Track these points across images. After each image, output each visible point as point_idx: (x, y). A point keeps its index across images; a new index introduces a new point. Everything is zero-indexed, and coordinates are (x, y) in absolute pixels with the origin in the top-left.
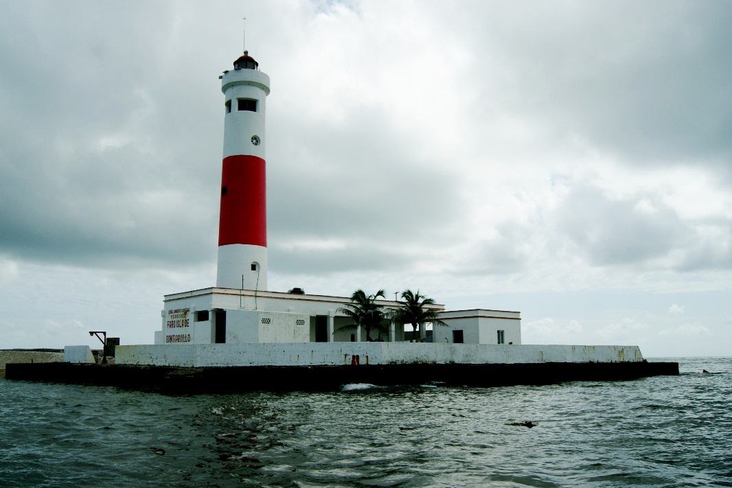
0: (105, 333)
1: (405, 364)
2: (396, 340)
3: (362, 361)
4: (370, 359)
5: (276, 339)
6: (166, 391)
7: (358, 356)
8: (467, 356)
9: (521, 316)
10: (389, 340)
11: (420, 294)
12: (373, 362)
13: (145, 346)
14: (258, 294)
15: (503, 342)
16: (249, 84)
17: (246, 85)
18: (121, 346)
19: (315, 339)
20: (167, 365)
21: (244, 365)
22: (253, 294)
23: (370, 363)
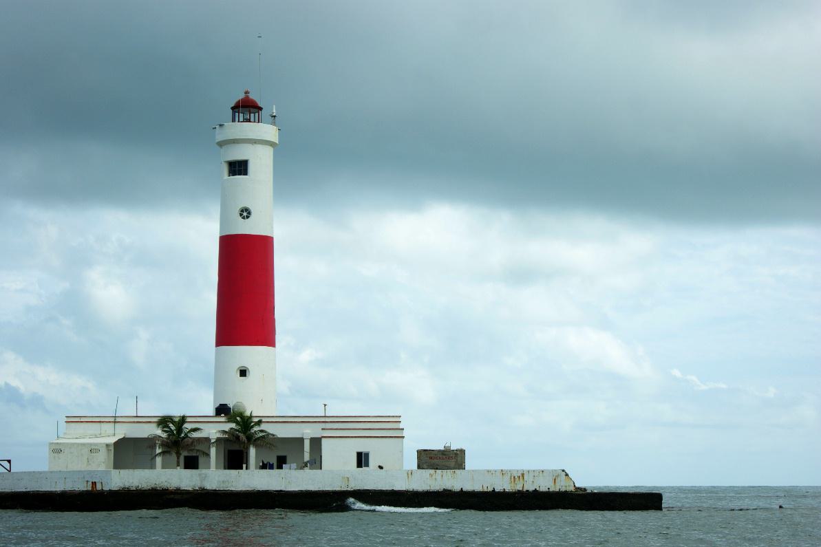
0: (9, 461)
1: (140, 490)
2: (163, 467)
3: (99, 487)
4: (541, 487)
5: (67, 467)
6: (149, 507)
7: (95, 482)
8: (223, 482)
9: (405, 433)
10: (273, 469)
11: (254, 415)
12: (106, 488)
13: (40, 473)
14: (118, 420)
15: (367, 465)
16: (234, 143)
17: (249, 143)
18: (468, 471)
19: (223, 465)
20: (558, 490)
21: (21, 490)
22: (112, 420)
23: (104, 489)
